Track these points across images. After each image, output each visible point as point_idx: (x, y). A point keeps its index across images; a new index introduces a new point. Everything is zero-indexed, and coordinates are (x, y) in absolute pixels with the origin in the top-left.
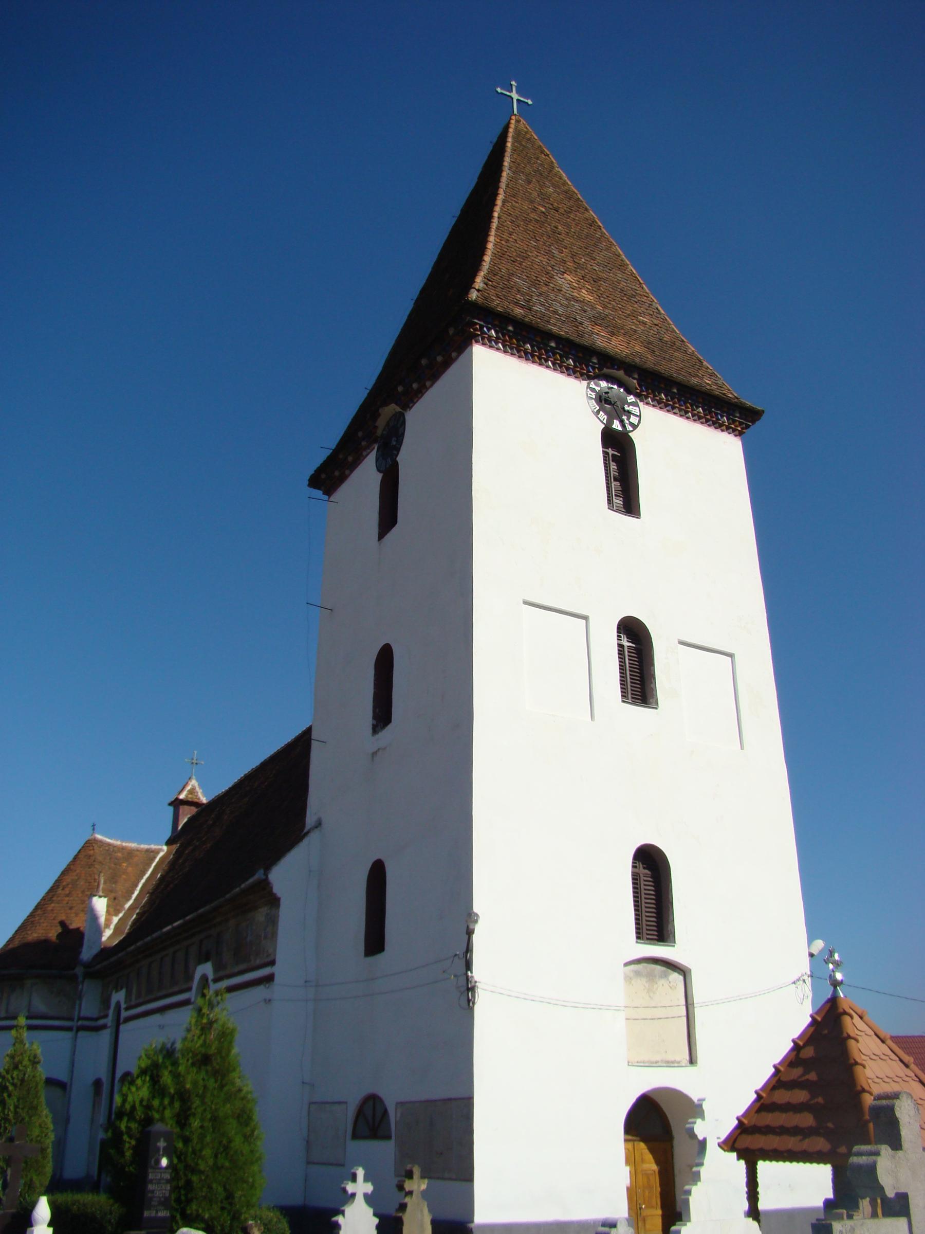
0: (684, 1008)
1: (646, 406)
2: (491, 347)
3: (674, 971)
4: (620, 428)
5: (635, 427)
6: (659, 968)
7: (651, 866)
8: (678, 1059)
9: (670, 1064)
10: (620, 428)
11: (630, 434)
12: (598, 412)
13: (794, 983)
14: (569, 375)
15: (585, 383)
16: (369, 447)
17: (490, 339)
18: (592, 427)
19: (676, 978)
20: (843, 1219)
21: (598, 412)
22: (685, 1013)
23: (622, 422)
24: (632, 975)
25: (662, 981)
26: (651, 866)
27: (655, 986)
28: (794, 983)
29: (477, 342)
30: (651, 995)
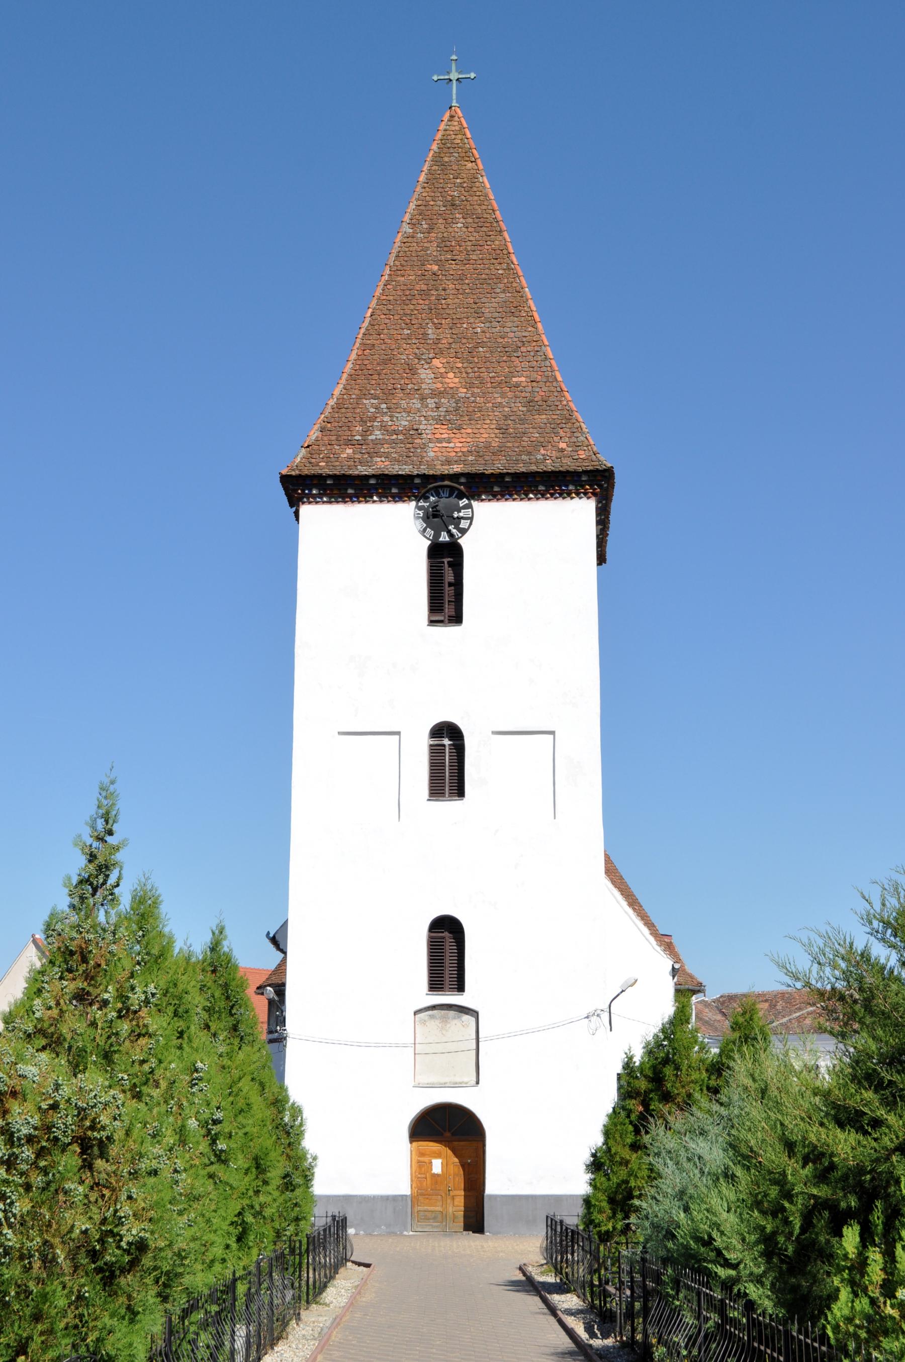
0: (474, 1041)
1: (481, 504)
2: (317, 503)
3: (467, 1014)
4: (447, 539)
5: (463, 531)
6: (452, 1013)
7: (447, 935)
8: (466, 1080)
9: (456, 1085)
10: (447, 539)
11: (459, 541)
12: (425, 530)
13: (587, 1017)
14: (396, 502)
15: (414, 503)
16: (642, 1063)
17: (314, 497)
18: (418, 547)
19: (469, 1019)
20: (444, 796)
21: (425, 530)
22: (474, 1047)
23: (449, 532)
24: (426, 1018)
25: (456, 1021)
26: (447, 935)
27: (448, 1026)
28: (587, 1017)
29: (303, 503)
30: (444, 1032)
